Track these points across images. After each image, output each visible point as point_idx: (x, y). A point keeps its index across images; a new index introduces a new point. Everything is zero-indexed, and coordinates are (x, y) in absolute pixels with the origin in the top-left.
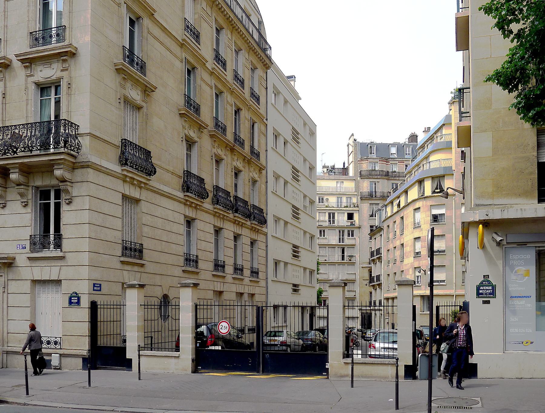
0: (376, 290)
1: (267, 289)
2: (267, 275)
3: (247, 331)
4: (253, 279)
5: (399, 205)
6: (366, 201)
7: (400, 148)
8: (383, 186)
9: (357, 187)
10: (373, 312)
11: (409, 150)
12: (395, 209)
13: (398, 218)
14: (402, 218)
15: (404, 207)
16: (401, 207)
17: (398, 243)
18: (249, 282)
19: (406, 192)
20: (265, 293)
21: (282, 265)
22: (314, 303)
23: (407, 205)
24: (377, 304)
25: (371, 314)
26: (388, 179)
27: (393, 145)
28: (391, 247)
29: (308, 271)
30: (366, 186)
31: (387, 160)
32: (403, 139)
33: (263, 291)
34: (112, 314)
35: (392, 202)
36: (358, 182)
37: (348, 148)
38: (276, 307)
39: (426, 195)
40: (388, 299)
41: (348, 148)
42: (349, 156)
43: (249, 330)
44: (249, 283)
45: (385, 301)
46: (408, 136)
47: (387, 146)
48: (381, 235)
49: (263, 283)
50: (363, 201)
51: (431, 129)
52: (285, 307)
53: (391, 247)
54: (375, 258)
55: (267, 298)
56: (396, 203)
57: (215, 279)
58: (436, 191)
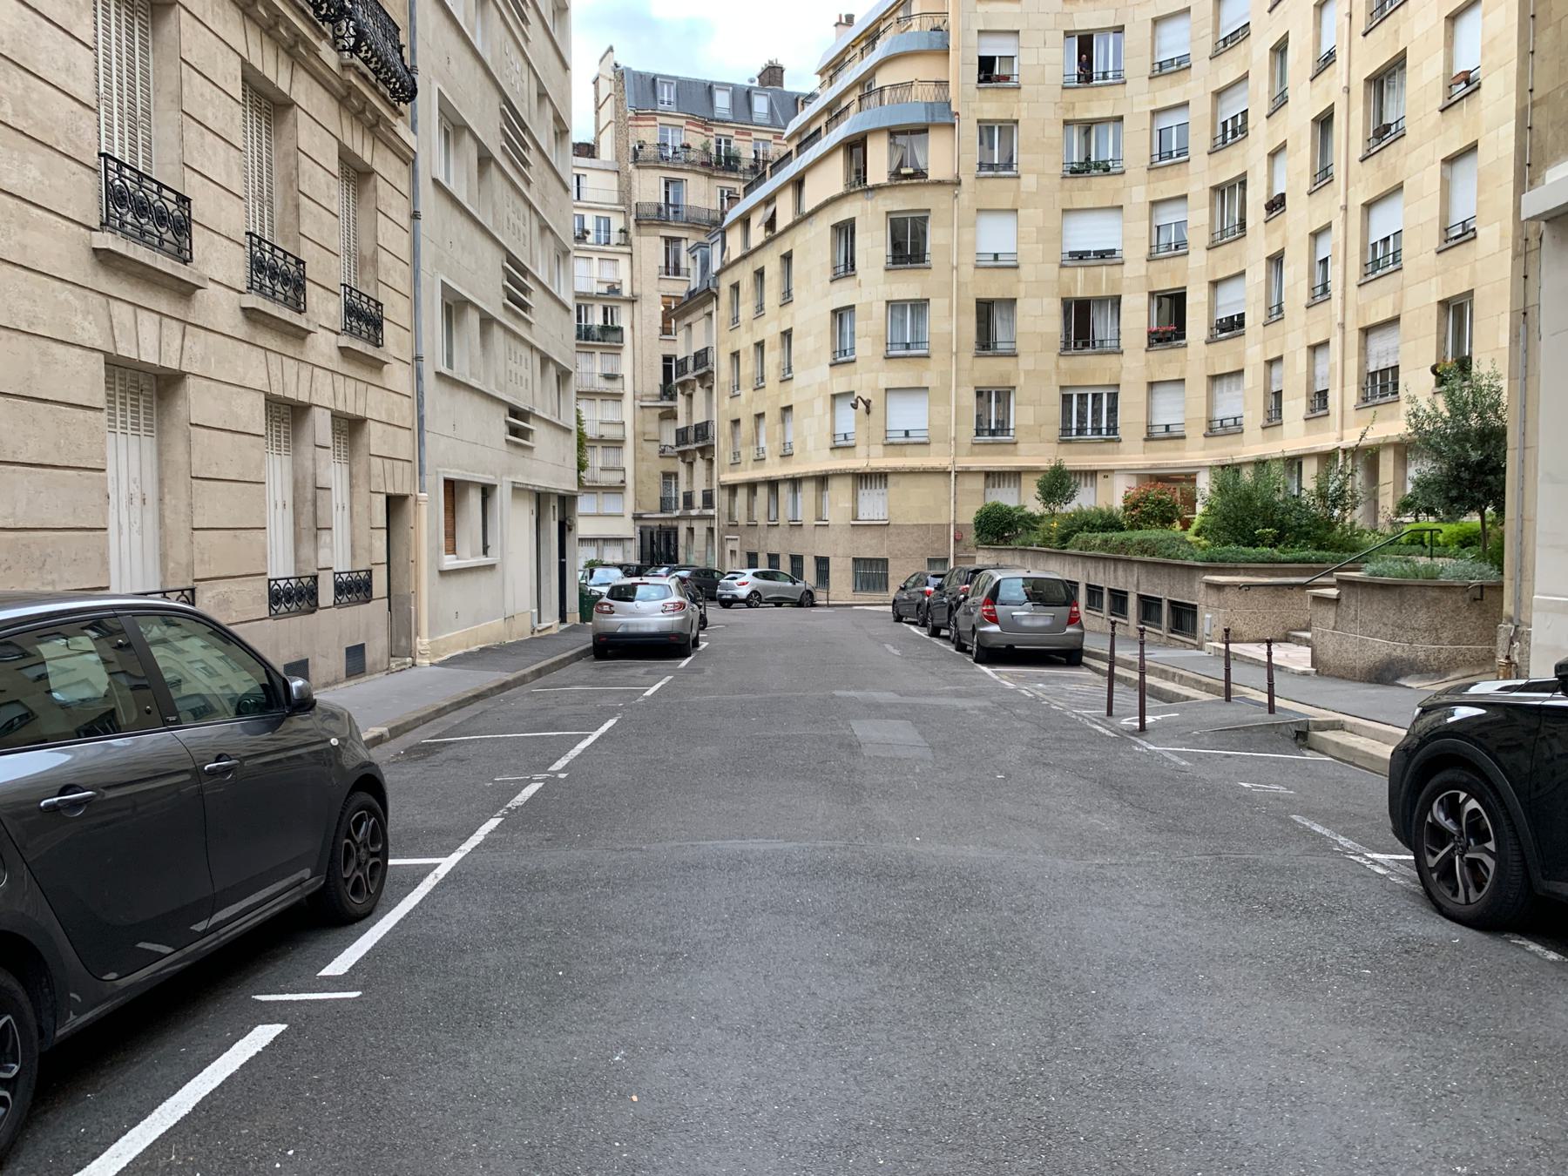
0: (691, 464)
1: (420, 405)
2: (417, 342)
3: (326, 594)
4: (359, 345)
5: (770, 224)
6: (652, 230)
7: (743, 98)
8: (700, 193)
9: (625, 192)
10: (682, 528)
11: (760, 105)
12: (758, 234)
13: (770, 262)
14: (787, 258)
15: (788, 229)
16: (779, 227)
17: (769, 331)
18: (335, 354)
19: (798, 183)
20: (409, 420)
21: (473, 319)
22: (568, 485)
23: (802, 219)
24: (698, 500)
25: (676, 530)
26: (710, 176)
27: (724, 86)
28: (745, 342)
29: (552, 369)
30: (649, 188)
31: (707, 123)
32: (745, 72)
33: (404, 412)
34: (125, 549)
35: (745, 221)
36: (629, 177)
37: (597, 88)
38: (453, 489)
39: (870, 182)
40: (733, 489)
41: (597, 88)
42: (598, 108)
43: (340, 589)
44: (336, 363)
45: (725, 495)
46: (759, 71)
47: (709, 89)
48: (710, 314)
49: (398, 376)
50: (643, 230)
51: (856, 20)
52: (487, 491)
53: (745, 342)
54: (690, 376)
55: (421, 443)
56: (757, 220)
57: (105, 283)
58: (903, 171)
